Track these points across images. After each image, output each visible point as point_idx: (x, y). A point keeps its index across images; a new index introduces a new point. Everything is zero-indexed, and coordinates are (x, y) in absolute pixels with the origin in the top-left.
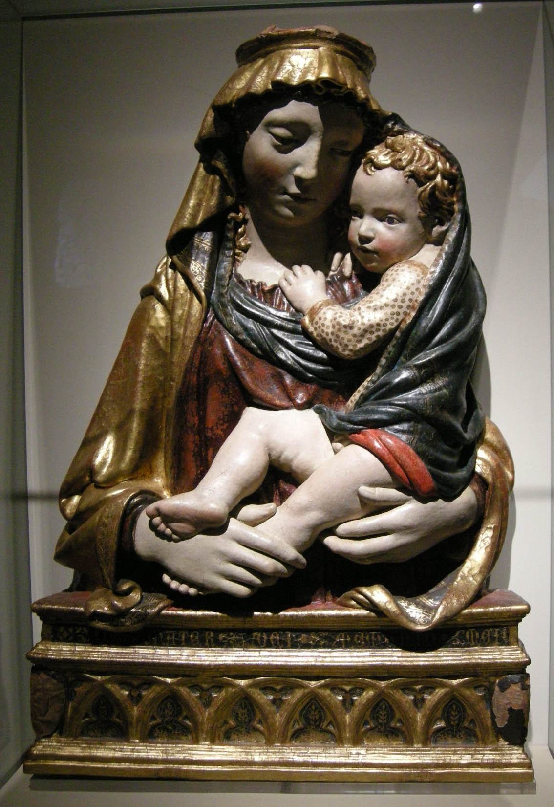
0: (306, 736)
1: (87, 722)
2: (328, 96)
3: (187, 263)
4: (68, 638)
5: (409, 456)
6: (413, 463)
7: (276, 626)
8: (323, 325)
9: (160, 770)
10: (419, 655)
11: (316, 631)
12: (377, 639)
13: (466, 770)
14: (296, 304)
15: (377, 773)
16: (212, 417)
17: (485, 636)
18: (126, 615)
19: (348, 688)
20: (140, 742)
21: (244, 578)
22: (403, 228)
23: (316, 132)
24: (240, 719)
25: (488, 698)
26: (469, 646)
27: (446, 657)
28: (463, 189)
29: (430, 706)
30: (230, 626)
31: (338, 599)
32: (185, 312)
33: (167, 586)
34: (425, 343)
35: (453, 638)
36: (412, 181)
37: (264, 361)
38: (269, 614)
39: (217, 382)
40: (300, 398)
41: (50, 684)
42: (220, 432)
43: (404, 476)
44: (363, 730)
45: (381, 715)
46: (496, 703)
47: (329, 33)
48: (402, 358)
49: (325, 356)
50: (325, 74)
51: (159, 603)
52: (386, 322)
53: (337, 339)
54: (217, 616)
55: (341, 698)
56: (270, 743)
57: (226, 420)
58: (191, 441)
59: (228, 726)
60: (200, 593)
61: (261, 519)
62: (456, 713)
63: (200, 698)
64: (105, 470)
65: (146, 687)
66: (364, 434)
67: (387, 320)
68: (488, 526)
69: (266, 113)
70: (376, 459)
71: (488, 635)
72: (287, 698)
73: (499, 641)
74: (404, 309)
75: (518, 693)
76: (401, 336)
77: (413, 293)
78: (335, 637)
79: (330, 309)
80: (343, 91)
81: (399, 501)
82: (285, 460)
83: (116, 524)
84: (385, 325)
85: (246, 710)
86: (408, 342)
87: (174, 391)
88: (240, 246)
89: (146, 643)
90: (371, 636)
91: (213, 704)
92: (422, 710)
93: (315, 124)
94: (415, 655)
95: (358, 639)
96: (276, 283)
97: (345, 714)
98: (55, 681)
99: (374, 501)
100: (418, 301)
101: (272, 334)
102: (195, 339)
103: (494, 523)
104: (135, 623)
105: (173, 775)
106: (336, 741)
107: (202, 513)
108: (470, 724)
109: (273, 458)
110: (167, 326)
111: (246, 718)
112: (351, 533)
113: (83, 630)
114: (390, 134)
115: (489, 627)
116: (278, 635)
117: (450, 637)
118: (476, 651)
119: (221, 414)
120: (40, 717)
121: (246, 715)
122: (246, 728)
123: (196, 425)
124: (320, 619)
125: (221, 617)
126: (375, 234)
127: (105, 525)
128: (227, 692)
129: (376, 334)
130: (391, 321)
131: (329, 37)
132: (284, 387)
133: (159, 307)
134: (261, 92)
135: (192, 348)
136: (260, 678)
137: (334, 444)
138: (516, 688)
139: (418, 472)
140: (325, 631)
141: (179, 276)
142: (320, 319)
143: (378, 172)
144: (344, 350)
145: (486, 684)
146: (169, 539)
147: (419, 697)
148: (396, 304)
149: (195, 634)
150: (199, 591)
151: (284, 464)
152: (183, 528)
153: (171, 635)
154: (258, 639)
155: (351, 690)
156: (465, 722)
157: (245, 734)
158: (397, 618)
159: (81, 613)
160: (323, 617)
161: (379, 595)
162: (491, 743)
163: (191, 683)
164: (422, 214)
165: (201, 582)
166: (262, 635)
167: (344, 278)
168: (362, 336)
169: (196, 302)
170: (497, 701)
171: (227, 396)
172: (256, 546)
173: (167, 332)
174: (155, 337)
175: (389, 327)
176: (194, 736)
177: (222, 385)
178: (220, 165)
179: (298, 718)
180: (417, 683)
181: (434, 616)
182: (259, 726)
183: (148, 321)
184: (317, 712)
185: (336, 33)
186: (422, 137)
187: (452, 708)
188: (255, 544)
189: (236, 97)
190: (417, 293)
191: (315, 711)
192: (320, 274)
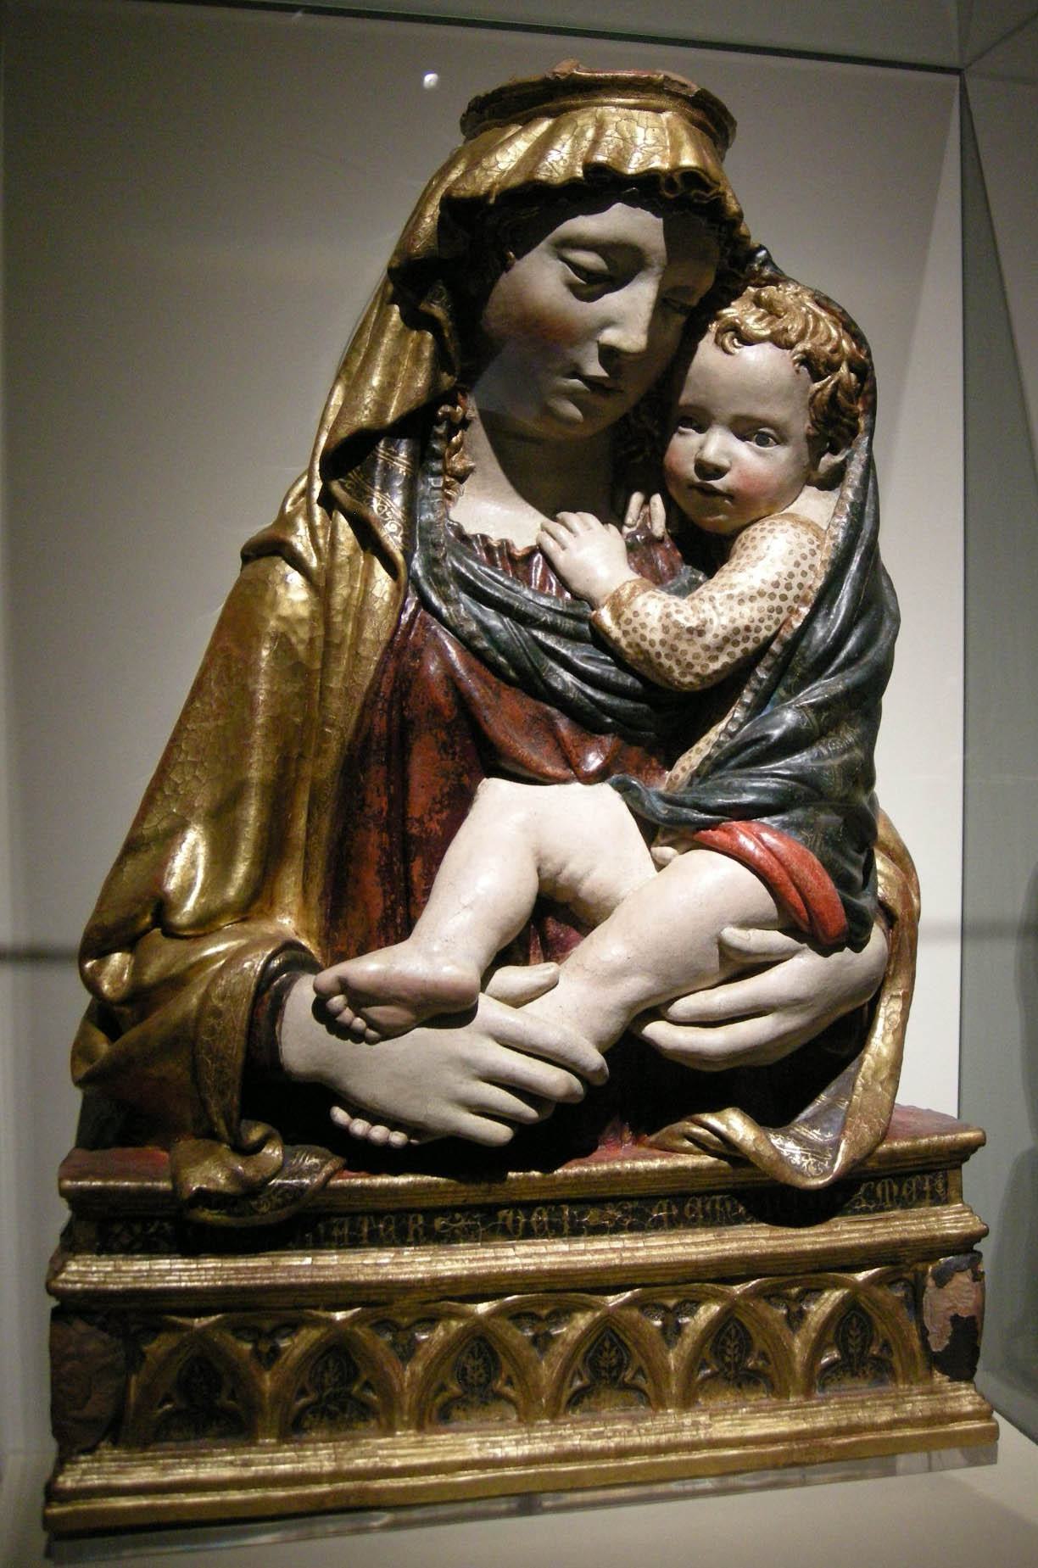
0: (592, 1399)
1: (168, 1414)
2: (682, 203)
3: (363, 495)
4: (132, 1244)
5: (812, 871)
6: (820, 884)
7: (545, 1196)
8: (643, 626)
9: (324, 1495)
10: (802, 1232)
11: (614, 1200)
12: (725, 1209)
13: (886, 1434)
14: (577, 585)
15: (924, 1435)
16: (419, 801)
17: (908, 1190)
18: (260, 1193)
19: (671, 1303)
20: (279, 1444)
21: (506, 1108)
22: (782, 454)
23: (653, 267)
24: (470, 1380)
25: (915, 1301)
26: (881, 1209)
27: (846, 1232)
28: (873, 391)
29: (817, 1322)
30: (459, 1201)
31: (653, 1138)
32: (357, 592)
33: (344, 1131)
34: (819, 667)
35: (856, 1196)
36: (804, 369)
37: (518, 690)
38: (536, 1174)
39: (430, 729)
40: (594, 761)
41: (92, 1341)
42: (435, 826)
43: (801, 907)
44: (700, 1377)
45: (851, 1336)
46: (928, 1307)
47: (684, 86)
48: (781, 691)
49: (638, 684)
50: (688, 160)
51: (323, 1166)
52: (760, 624)
53: (671, 653)
54: (437, 1185)
55: (658, 1323)
56: (527, 1418)
57: (446, 802)
58: (374, 842)
59: (447, 1394)
60: (412, 1141)
61: (532, 993)
62: (859, 1332)
63: (393, 1345)
64: (190, 904)
65: (284, 1332)
66: (729, 831)
67: (761, 620)
68: (894, 993)
69: (561, 222)
70: (754, 877)
71: (914, 1188)
72: (559, 1331)
73: (932, 1198)
74: (790, 602)
75: (968, 1288)
76: (783, 650)
77: (804, 574)
78: (651, 1210)
79: (654, 597)
80: (711, 193)
81: (784, 953)
82: (568, 880)
83: (243, 1009)
84: (758, 630)
85: (481, 1360)
86: (793, 663)
87: (334, 747)
88: (452, 469)
89: (290, 1244)
90: (714, 1202)
91: (420, 1353)
92: (802, 1331)
93: (655, 252)
94: (794, 1233)
95: (692, 1210)
96: (534, 543)
97: (667, 1352)
98: (106, 1336)
99: (748, 953)
100: (814, 589)
101: (535, 639)
102: (383, 645)
103: (903, 987)
104: (279, 1207)
105: (353, 1501)
106: (649, 1403)
107: (436, 985)
108: (881, 1350)
109: (546, 875)
110: (313, 617)
111: (480, 1376)
112: (700, 1015)
113: (163, 1228)
114: (753, 282)
115: (911, 1174)
116: (545, 1213)
117: (848, 1198)
118: (896, 1218)
119: (438, 791)
120: (75, 1413)
121: (481, 1371)
122: (481, 1396)
123: (384, 814)
124: (630, 1178)
125: (445, 1184)
126: (731, 463)
127: (217, 1014)
128: (446, 1330)
129: (742, 646)
130: (767, 623)
131: (683, 92)
132: (559, 743)
133: (295, 578)
134: (559, 181)
135: (379, 663)
136: (509, 1299)
137: (658, 850)
138: (963, 1279)
139: (826, 899)
140: (631, 1199)
141: (342, 520)
142: (636, 614)
143: (746, 348)
144: (683, 674)
145: (908, 1275)
146: (358, 1037)
147: (795, 1309)
148: (778, 592)
149: (388, 1223)
150: (410, 1137)
151: (564, 888)
152: (393, 1015)
153: (341, 1226)
154: (509, 1222)
155: (675, 1307)
156: (872, 1348)
157: (478, 1408)
158: (775, 1168)
159: (164, 1194)
160: (635, 1173)
161: (736, 1125)
162: (920, 1380)
163: (376, 1317)
164: (811, 432)
165: (421, 1119)
166: (516, 1214)
167: (652, 541)
168: (720, 648)
169: (380, 573)
170: (931, 1305)
171: (450, 757)
172: (533, 1047)
173: (312, 629)
174: (289, 640)
175: (764, 633)
176: (383, 1420)
177: (443, 736)
178: (438, 311)
179: (580, 1367)
180: (792, 1285)
181: (834, 1160)
182: (507, 1390)
183: (274, 604)
184: (613, 1353)
185: (696, 89)
186: (810, 292)
187: (850, 1323)
188: (533, 1042)
189: (497, 186)
190: (811, 575)
191: (609, 1352)
192: (613, 529)
